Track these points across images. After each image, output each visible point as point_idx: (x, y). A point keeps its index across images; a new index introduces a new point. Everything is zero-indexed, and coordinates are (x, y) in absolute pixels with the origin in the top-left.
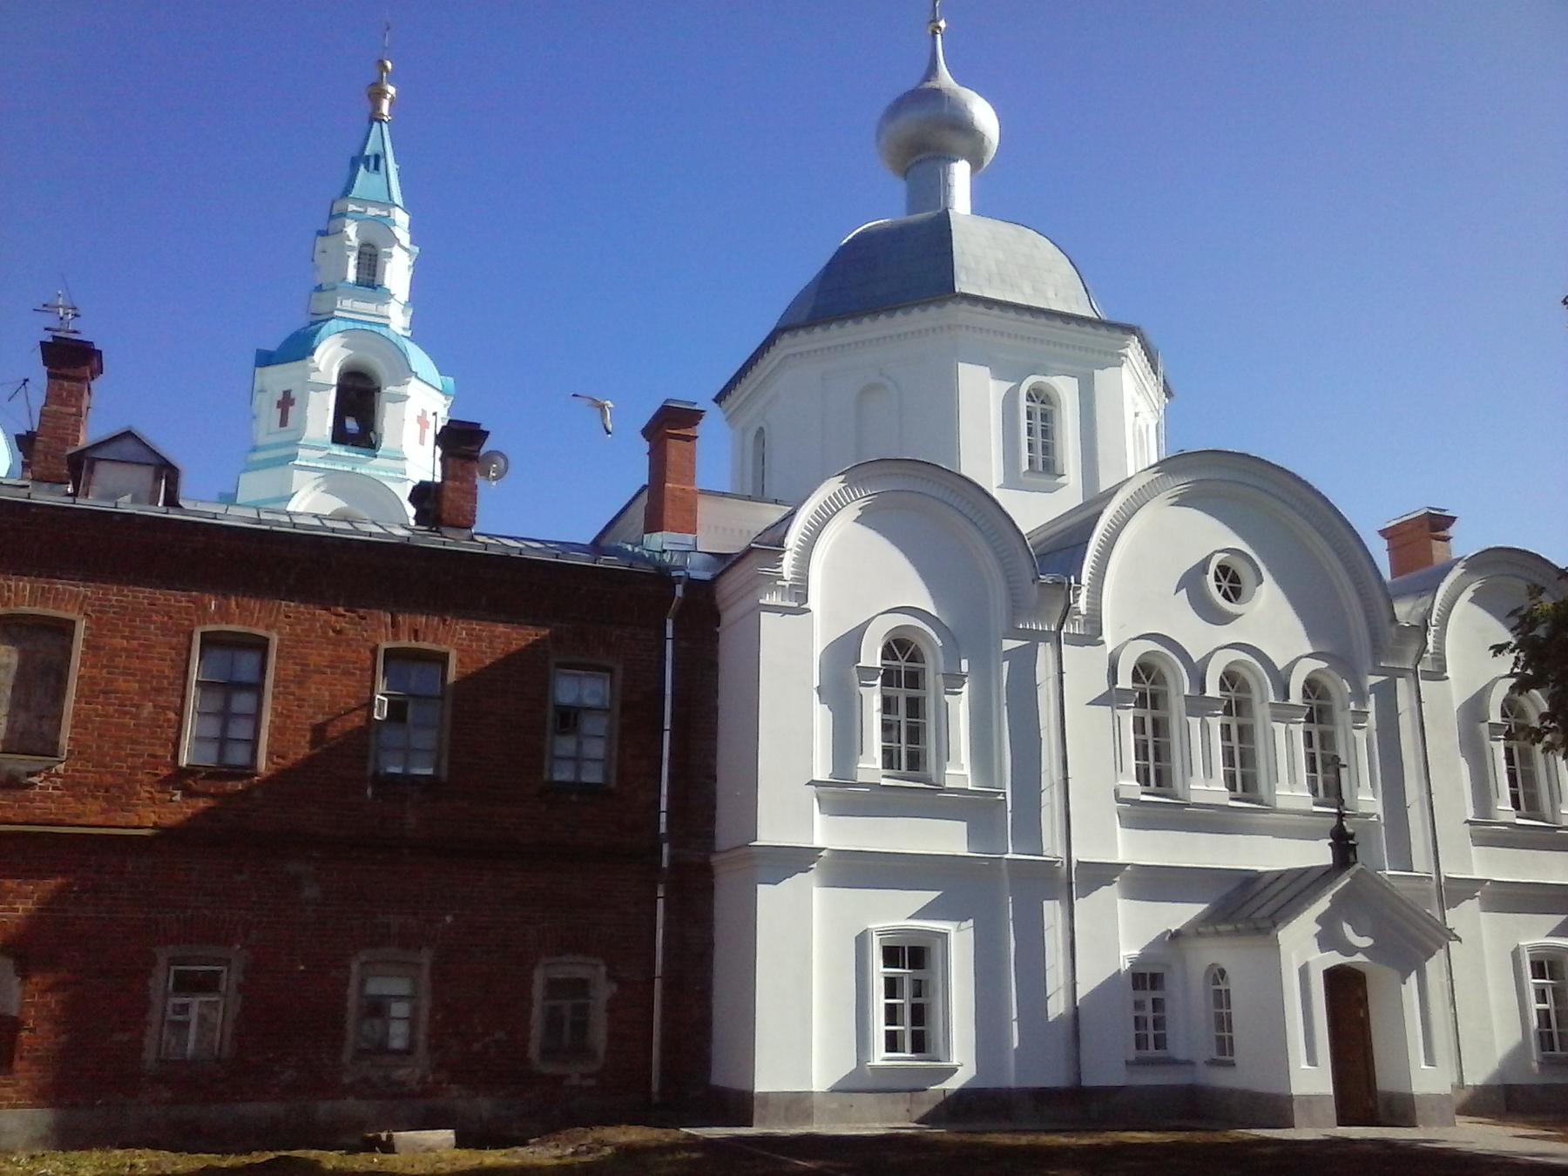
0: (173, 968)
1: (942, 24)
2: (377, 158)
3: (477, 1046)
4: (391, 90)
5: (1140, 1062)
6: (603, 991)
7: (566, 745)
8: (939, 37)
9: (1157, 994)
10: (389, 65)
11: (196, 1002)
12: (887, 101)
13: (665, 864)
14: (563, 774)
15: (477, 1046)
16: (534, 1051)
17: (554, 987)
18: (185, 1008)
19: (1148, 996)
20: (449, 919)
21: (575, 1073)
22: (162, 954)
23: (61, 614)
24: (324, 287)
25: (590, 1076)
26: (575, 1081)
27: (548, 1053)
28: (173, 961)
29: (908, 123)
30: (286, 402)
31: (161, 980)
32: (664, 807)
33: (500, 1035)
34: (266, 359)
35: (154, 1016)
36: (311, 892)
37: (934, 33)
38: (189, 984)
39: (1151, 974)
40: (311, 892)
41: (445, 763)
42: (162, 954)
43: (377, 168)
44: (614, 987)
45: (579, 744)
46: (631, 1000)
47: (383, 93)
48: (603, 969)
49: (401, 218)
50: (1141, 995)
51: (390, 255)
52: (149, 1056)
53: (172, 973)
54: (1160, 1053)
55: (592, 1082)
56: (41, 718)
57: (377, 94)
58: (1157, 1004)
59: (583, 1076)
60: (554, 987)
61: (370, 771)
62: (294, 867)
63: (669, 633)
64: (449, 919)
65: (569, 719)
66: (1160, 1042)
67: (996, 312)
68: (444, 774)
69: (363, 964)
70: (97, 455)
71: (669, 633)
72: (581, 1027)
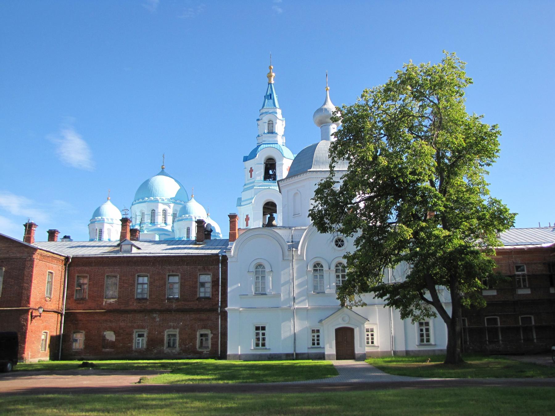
0: (137, 333)
1: (329, 88)
2: (271, 95)
3: (187, 346)
4: (273, 74)
5: (420, 345)
6: (210, 336)
7: (202, 290)
8: (328, 92)
9: (318, 334)
10: (272, 67)
11: (141, 339)
12: (313, 116)
13: (219, 312)
14: (202, 295)
15: (187, 346)
16: (197, 347)
17: (202, 335)
18: (139, 340)
19: (316, 334)
20: (181, 323)
21: (205, 351)
22: (135, 331)
23: (116, 274)
24: (260, 135)
25: (208, 351)
26: (205, 352)
27: (199, 348)
28: (136, 332)
29: (318, 117)
30: (251, 171)
31: (135, 335)
32: (220, 301)
33: (191, 344)
34: (246, 159)
35: (134, 341)
36: (158, 319)
37: (327, 91)
38: (140, 336)
39: (316, 330)
40: (158, 319)
41: (179, 295)
42: (135, 331)
43: (271, 98)
44: (212, 335)
45: (205, 289)
46: (215, 337)
47: (271, 76)
48: (210, 332)
49: (279, 111)
50: (314, 334)
51: (276, 123)
52: (134, 348)
53: (137, 335)
54: (318, 346)
55: (209, 353)
56: (114, 292)
57: (270, 76)
58: (318, 336)
59: (207, 351)
60: (202, 335)
61: (166, 297)
62: (155, 315)
63: (220, 266)
64: (181, 323)
65: (203, 285)
66: (263, 345)
67: (319, 173)
68: (179, 297)
69: (167, 332)
70: (122, 244)
71: (220, 266)
72: (174, 343)
